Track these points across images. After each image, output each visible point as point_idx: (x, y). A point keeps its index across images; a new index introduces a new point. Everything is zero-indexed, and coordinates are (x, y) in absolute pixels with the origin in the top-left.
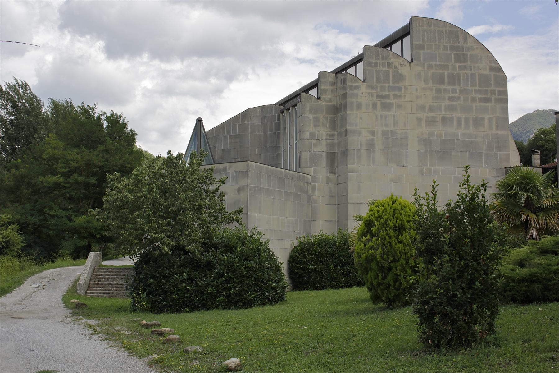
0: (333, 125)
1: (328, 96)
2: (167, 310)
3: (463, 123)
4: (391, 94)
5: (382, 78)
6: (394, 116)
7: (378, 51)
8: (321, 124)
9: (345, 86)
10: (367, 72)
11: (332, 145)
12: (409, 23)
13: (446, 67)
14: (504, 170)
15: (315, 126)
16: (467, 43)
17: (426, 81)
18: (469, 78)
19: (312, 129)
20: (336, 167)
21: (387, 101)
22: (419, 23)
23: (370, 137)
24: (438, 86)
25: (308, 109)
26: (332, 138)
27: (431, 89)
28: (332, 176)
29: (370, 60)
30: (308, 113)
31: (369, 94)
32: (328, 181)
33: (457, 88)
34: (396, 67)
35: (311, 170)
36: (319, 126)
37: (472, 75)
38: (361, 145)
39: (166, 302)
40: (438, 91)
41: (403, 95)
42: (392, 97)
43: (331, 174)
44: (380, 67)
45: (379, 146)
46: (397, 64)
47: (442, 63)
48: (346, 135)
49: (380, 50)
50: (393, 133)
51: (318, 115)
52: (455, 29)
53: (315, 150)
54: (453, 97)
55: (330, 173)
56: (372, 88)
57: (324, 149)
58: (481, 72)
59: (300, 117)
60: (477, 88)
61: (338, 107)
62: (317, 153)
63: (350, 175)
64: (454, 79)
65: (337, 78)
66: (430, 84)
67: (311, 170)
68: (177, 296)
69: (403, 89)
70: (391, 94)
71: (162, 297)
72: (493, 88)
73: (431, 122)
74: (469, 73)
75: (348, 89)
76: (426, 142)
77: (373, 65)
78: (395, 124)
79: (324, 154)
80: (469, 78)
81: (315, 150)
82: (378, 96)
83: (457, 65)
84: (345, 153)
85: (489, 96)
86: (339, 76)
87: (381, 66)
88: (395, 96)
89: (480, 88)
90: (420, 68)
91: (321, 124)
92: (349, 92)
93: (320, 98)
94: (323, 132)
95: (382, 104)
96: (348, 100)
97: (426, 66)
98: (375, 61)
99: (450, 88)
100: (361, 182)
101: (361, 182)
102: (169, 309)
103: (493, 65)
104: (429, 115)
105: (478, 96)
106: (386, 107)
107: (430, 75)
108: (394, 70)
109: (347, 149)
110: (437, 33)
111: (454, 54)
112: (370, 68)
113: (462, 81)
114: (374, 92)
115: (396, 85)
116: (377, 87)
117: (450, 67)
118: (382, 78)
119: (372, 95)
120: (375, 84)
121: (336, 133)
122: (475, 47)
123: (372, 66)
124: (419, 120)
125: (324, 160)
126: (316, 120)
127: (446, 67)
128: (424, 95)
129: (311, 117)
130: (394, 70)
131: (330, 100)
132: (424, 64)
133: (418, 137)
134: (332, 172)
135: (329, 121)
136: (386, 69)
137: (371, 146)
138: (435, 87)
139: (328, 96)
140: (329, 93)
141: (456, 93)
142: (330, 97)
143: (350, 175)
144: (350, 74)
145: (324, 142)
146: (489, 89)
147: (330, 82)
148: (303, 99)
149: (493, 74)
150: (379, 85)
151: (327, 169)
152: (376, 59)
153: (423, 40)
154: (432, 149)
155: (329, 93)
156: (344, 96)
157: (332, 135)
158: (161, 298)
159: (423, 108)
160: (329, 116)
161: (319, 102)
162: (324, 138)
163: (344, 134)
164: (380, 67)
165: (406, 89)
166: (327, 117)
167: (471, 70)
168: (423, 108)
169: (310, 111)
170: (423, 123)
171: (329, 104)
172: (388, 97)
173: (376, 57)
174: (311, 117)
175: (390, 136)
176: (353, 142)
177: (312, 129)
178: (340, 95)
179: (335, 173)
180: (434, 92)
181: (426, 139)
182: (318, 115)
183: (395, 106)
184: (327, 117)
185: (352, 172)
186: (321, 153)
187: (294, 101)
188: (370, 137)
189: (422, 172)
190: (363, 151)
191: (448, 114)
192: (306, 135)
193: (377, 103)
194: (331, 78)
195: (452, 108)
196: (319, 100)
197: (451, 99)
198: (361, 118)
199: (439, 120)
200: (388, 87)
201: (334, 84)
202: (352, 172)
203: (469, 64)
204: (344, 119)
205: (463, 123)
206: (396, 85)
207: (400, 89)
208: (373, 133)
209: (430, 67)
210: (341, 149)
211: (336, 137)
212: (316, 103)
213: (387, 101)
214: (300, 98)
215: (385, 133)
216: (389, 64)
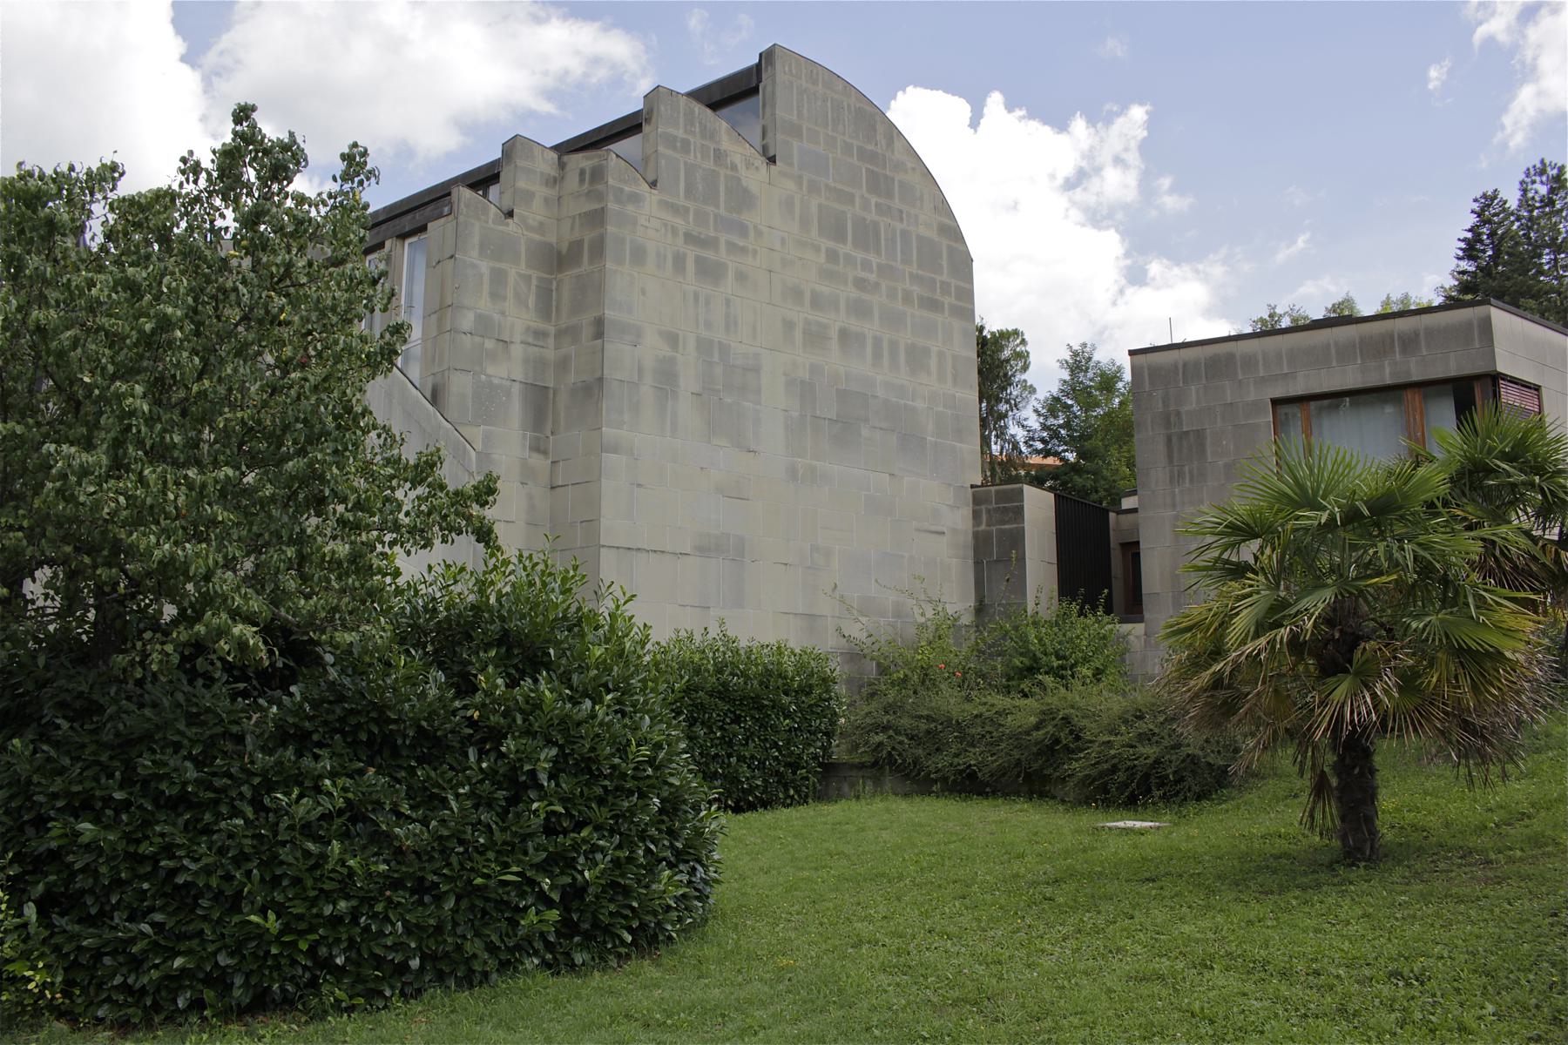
0: (546, 303)
1: (534, 212)
2: (197, 1005)
3: (886, 353)
4: (723, 238)
5: (700, 187)
6: (728, 302)
7: (692, 112)
8: (510, 294)
9: (600, 187)
10: (663, 162)
11: (539, 365)
12: (759, 66)
13: (850, 199)
14: (970, 491)
15: (496, 296)
16: (893, 151)
17: (805, 223)
18: (898, 239)
19: (484, 304)
20: (549, 434)
21: (708, 254)
22: (790, 65)
23: (666, 351)
24: (832, 244)
25: (476, 240)
26: (541, 343)
27: (817, 249)
28: (537, 461)
29: (671, 130)
30: (475, 253)
31: (666, 225)
32: (527, 474)
33: (874, 260)
34: (734, 167)
35: (476, 433)
36: (504, 298)
37: (904, 233)
38: (640, 370)
39: (188, 953)
40: (832, 256)
41: (751, 247)
42: (723, 247)
43: (535, 455)
44: (695, 157)
45: (688, 381)
46: (737, 159)
47: (840, 187)
48: (599, 334)
49: (699, 109)
50: (724, 349)
51: (503, 266)
52: (868, 108)
53: (491, 370)
54: (863, 280)
55: (531, 448)
56: (675, 209)
57: (518, 374)
58: (923, 231)
59: (450, 264)
60: (915, 269)
61: (564, 251)
62: (496, 381)
63: (609, 458)
64: (867, 236)
65: (562, 165)
66: (814, 232)
67: (476, 433)
68: (271, 916)
69: (752, 234)
70: (723, 238)
71: (153, 925)
72: (945, 278)
73: (815, 337)
74: (899, 226)
75: (611, 197)
76: (804, 390)
77: (679, 145)
78: (730, 324)
79: (516, 389)
80: (898, 239)
81: (491, 370)
82: (690, 238)
83: (874, 200)
84: (592, 390)
85: (938, 296)
86: (579, 161)
87: (699, 155)
88: (732, 247)
89: (920, 272)
90: (790, 185)
91: (510, 294)
92: (612, 206)
93: (510, 214)
94: (518, 318)
95: (699, 261)
96: (611, 229)
97: (805, 184)
98: (685, 136)
99: (859, 255)
100: (639, 485)
101: (639, 485)
102: (209, 995)
103: (947, 221)
104: (810, 317)
105: (916, 290)
106: (710, 272)
107: (814, 210)
108: (729, 173)
109: (601, 379)
110: (829, 104)
111: (867, 169)
112: (669, 152)
113: (883, 242)
114: (679, 222)
115: (735, 216)
116: (687, 210)
117: (857, 200)
118: (700, 187)
119: (674, 231)
120: (681, 201)
121: (552, 329)
122: (909, 165)
123: (674, 149)
124: (789, 325)
125: (516, 409)
126: (498, 277)
127: (850, 199)
128: (801, 259)
129: (485, 267)
130: (729, 173)
131: (541, 228)
132: (800, 177)
133: (785, 374)
134: (538, 448)
135: (533, 287)
136: (710, 164)
137: (667, 377)
138: (826, 244)
139: (534, 212)
140: (537, 204)
141: (871, 271)
142: (538, 217)
143: (609, 458)
144: (617, 156)
145: (517, 351)
146: (938, 278)
147: (542, 173)
148: (462, 206)
149: (945, 242)
150: (691, 205)
151: (524, 436)
152: (686, 132)
153: (800, 114)
154: (818, 413)
155: (537, 204)
156: (597, 218)
157: (540, 335)
158: (146, 928)
159: (796, 293)
160: (535, 274)
161: (507, 225)
162: (518, 338)
163: (587, 332)
164: (695, 157)
165: (759, 234)
166: (530, 276)
167: (901, 219)
168: (796, 293)
169: (483, 246)
170: (798, 335)
171: (537, 237)
172: (710, 243)
173: (685, 126)
174: (485, 267)
175: (716, 358)
176: (621, 358)
177: (484, 304)
178: (574, 217)
179: (545, 453)
180: (822, 259)
181: (802, 382)
182: (503, 266)
183: (731, 274)
184: (530, 276)
185: (615, 450)
186: (508, 383)
187: (418, 217)
188: (666, 351)
189: (793, 473)
190: (647, 391)
191: (854, 324)
192: (467, 321)
193: (685, 255)
194: (546, 164)
195: (860, 310)
196: (510, 221)
197: (860, 284)
198: (643, 292)
199: (834, 334)
200: (716, 216)
201: (554, 182)
202: (615, 450)
203: (897, 203)
204: (590, 290)
205: (886, 353)
206: (735, 216)
207: (743, 230)
208: (673, 340)
209: (814, 188)
210: (572, 378)
211: (551, 341)
212: (501, 228)
213: (708, 254)
214: (451, 203)
215: (704, 346)
216: (719, 156)
